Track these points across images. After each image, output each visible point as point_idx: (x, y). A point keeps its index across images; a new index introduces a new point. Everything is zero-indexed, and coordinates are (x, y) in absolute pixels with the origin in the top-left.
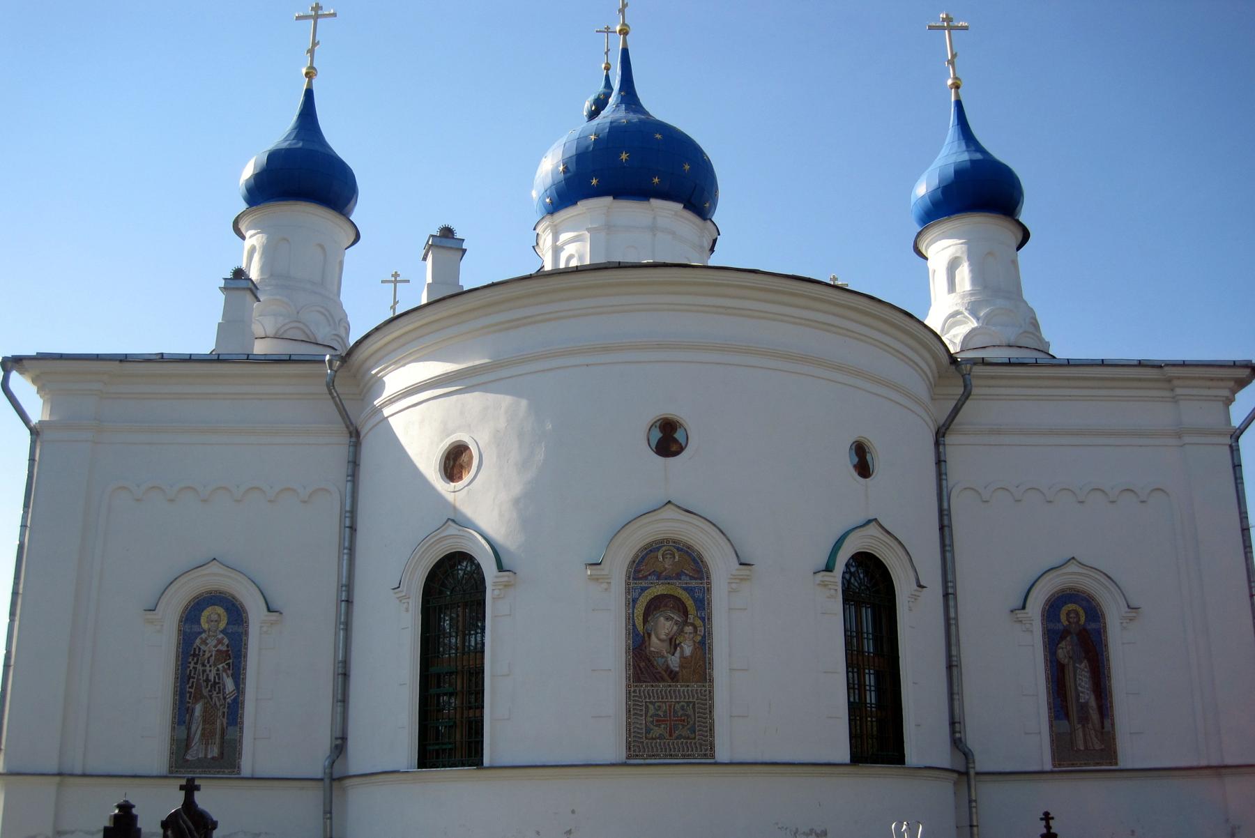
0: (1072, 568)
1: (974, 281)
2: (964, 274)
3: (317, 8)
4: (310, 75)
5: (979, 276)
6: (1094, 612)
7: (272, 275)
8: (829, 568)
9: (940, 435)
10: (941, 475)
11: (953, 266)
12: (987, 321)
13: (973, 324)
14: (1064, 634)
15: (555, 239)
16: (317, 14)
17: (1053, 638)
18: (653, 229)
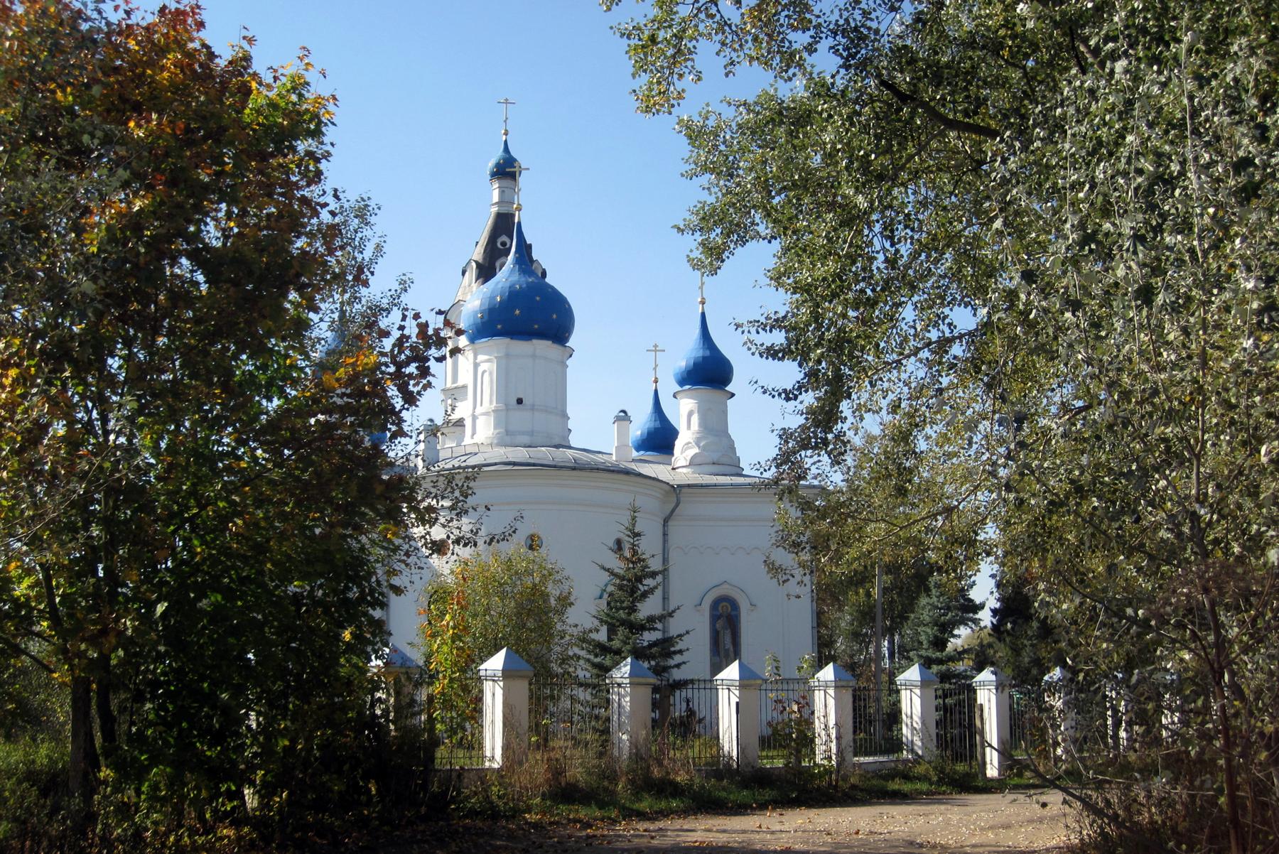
0: (725, 586)
1: (700, 425)
2: (695, 419)
3: (656, 346)
4: (656, 382)
5: (704, 423)
6: (734, 605)
7: (507, 432)
8: (601, 597)
9: (666, 521)
10: (665, 541)
11: (690, 414)
12: (704, 449)
13: (696, 450)
14: (719, 617)
15: (475, 358)
16: (656, 349)
17: (714, 618)
18: (534, 356)
